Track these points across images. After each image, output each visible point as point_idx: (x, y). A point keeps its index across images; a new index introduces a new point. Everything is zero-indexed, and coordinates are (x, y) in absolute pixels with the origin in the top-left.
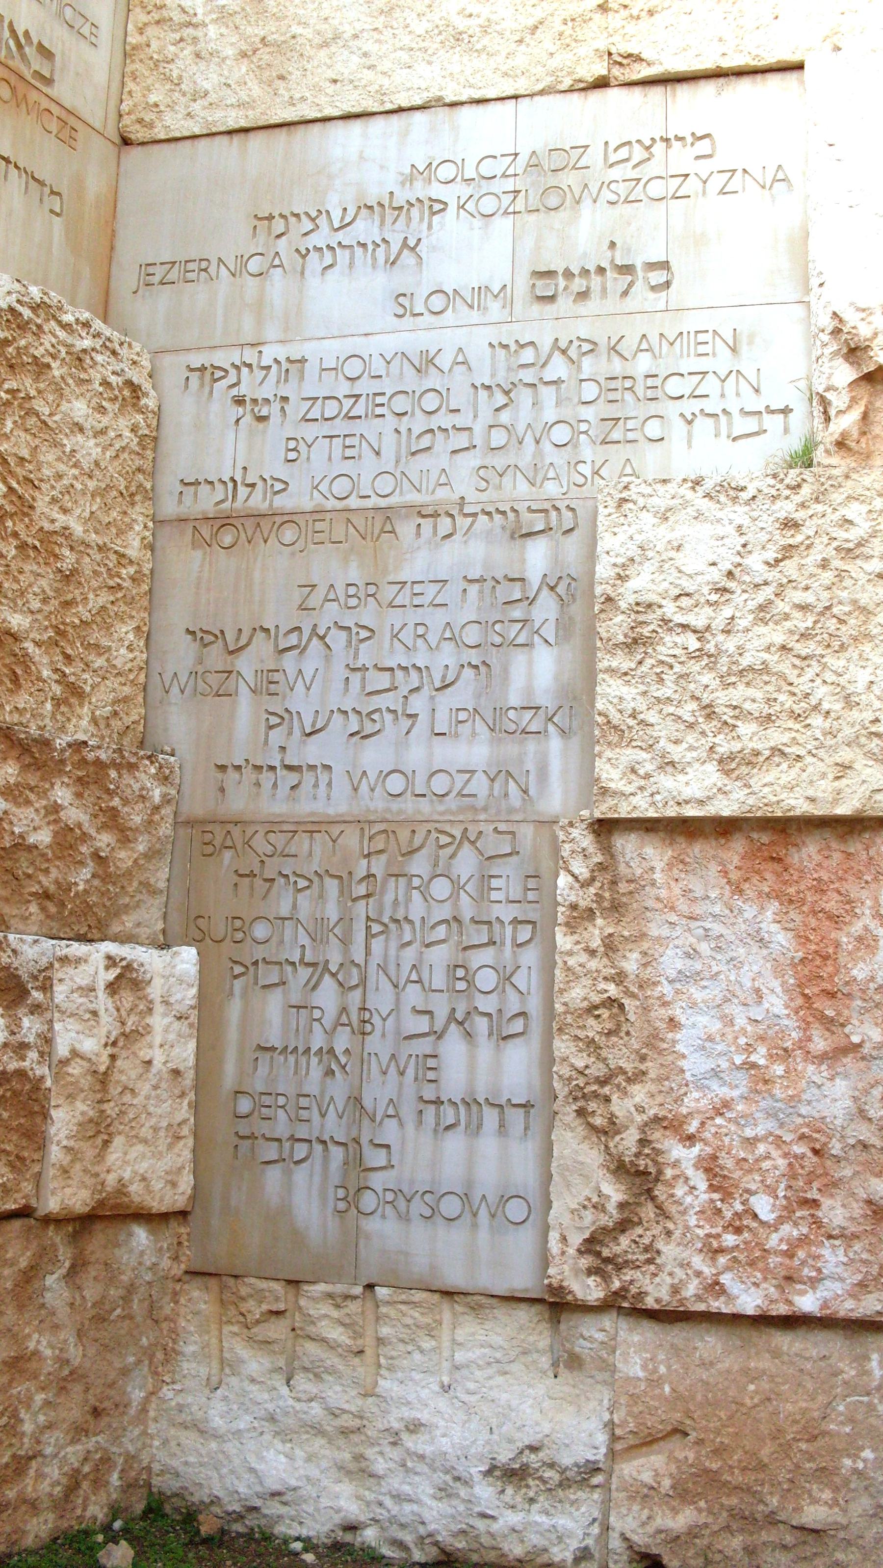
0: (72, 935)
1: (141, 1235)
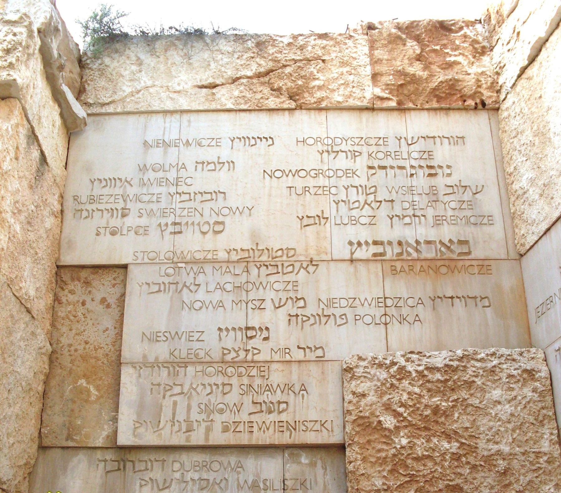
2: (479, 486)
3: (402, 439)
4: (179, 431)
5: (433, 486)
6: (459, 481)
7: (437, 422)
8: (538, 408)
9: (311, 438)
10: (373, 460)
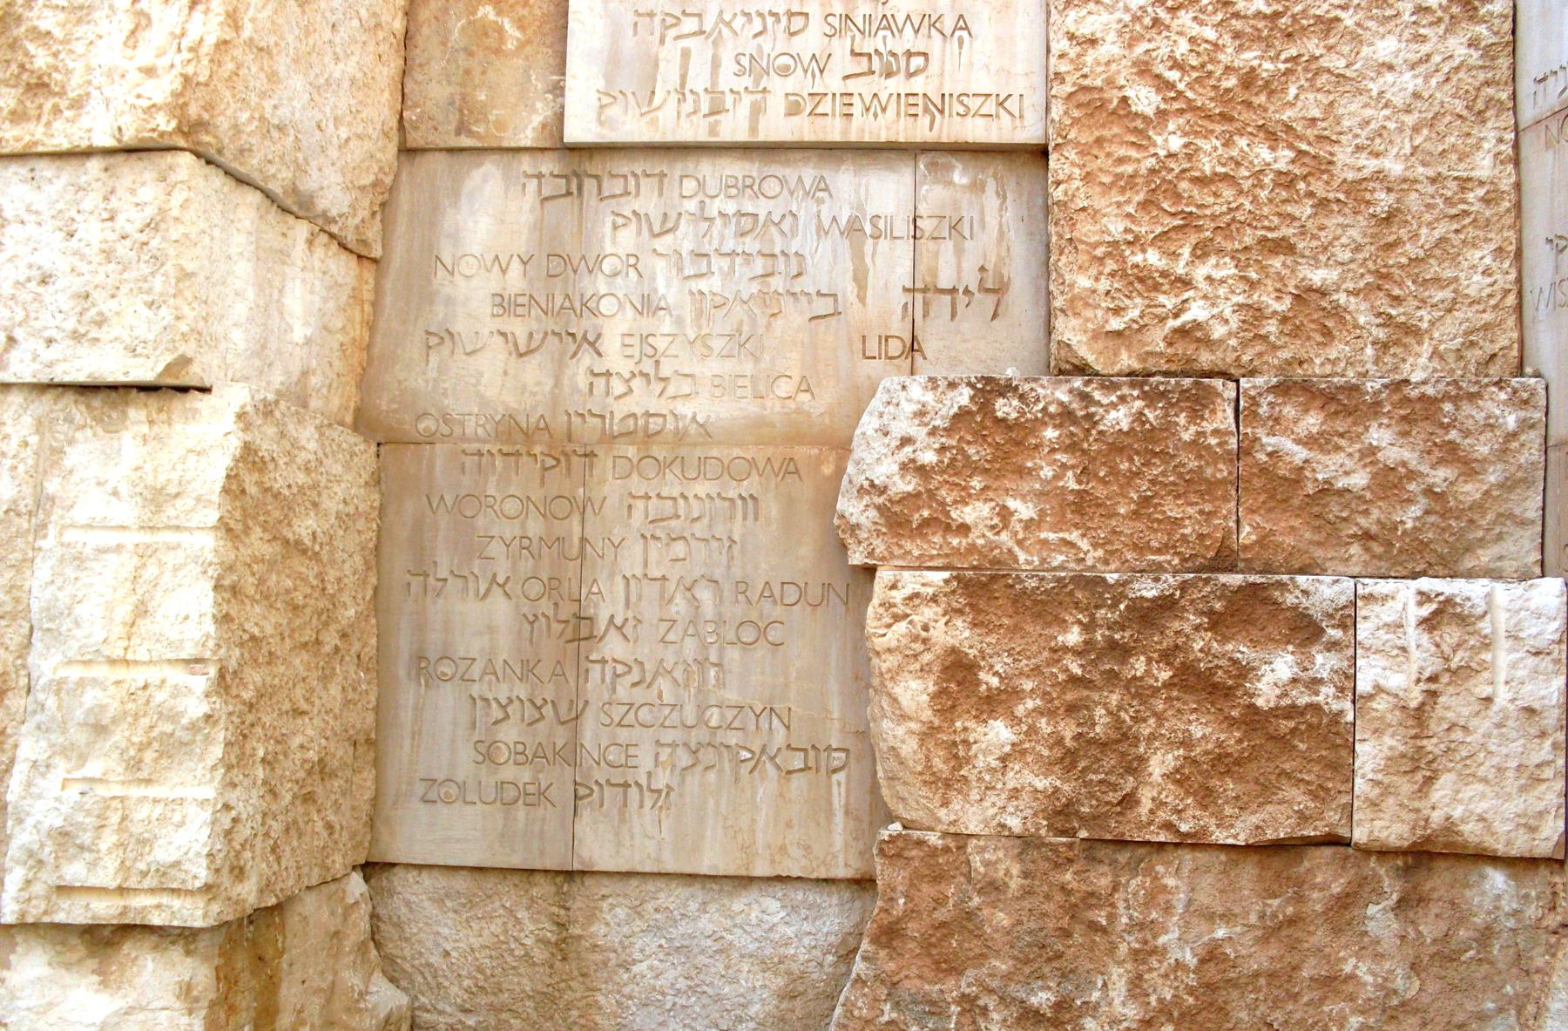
0: (1404, 573)
1: (1497, 879)
2: (1330, 243)
3: (1171, 138)
4: (695, 112)
5: (1232, 239)
6: (1288, 231)
7: (1248, 104)
8: (1477, 84)
9: (977, 131)
10: (1107, 179)
